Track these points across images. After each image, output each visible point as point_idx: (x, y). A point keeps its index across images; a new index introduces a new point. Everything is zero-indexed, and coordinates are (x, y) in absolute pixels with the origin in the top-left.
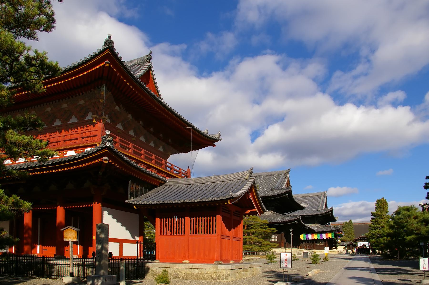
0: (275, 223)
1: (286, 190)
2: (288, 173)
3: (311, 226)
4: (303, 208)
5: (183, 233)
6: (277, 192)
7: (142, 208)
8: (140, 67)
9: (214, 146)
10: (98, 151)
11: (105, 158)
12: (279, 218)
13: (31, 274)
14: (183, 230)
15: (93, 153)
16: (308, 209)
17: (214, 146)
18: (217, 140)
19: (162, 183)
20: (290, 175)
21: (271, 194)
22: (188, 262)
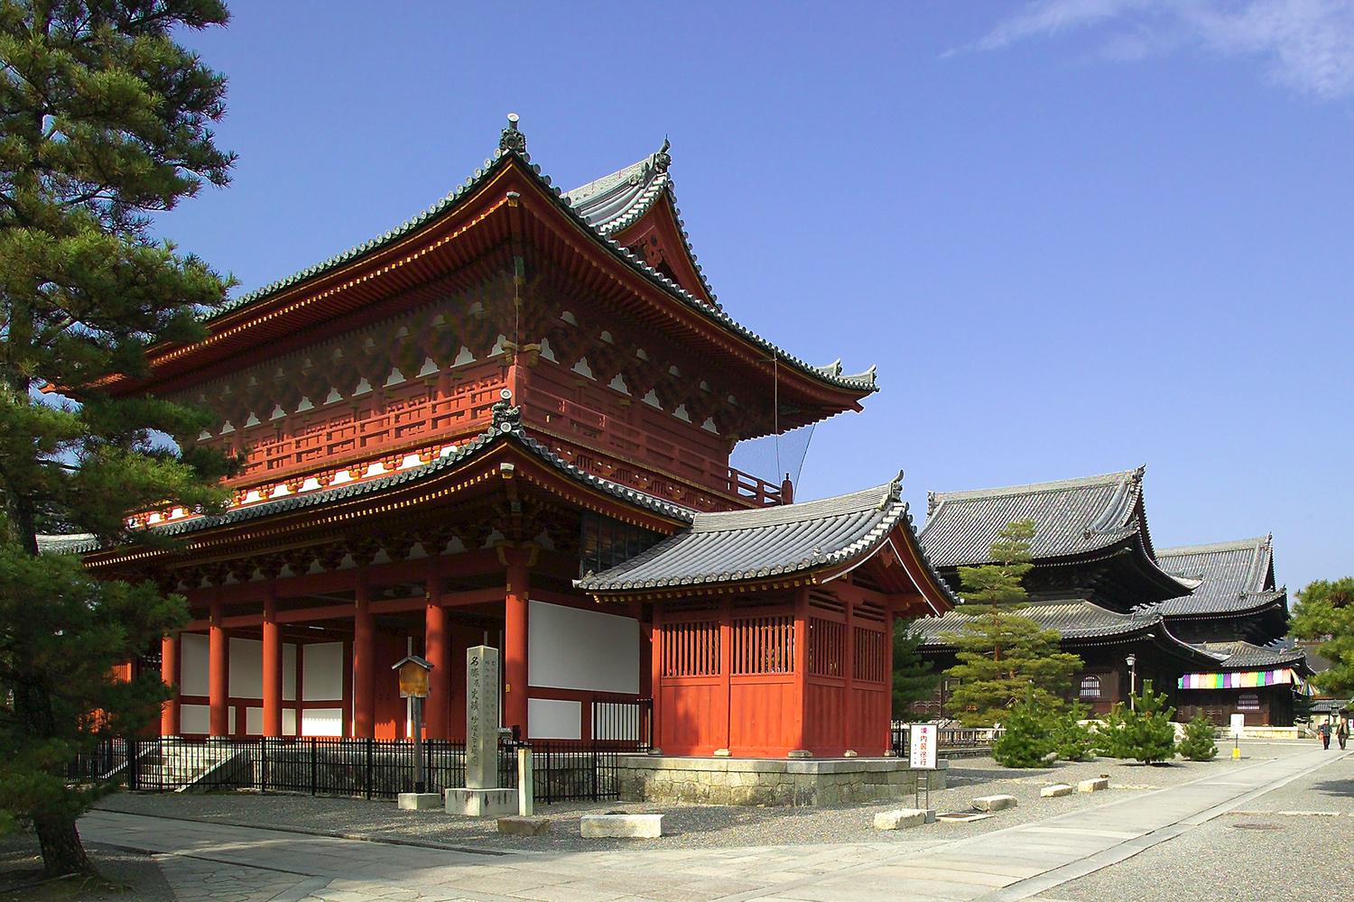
0: (1078, 640)
1: (1124, 536)
2: (1137, 479)
3: (1214, 650)
4: (1186, 591)
5: (789, 668)
6: (1098, 542)
7: (659, 596)
8: (638, 191)
9: (859, 408)
10: (486, 447)
11: (504, 466)
12: (1110, 624)
13: (647, 748)
14: (817, 658)
15: (466, 459)
16: (1206, 598)
17: (859, 408)
18: (865, 392)
19: (684, 527)
20: (1145, 482)
21: (1083, 546)
22: (726, 752)
